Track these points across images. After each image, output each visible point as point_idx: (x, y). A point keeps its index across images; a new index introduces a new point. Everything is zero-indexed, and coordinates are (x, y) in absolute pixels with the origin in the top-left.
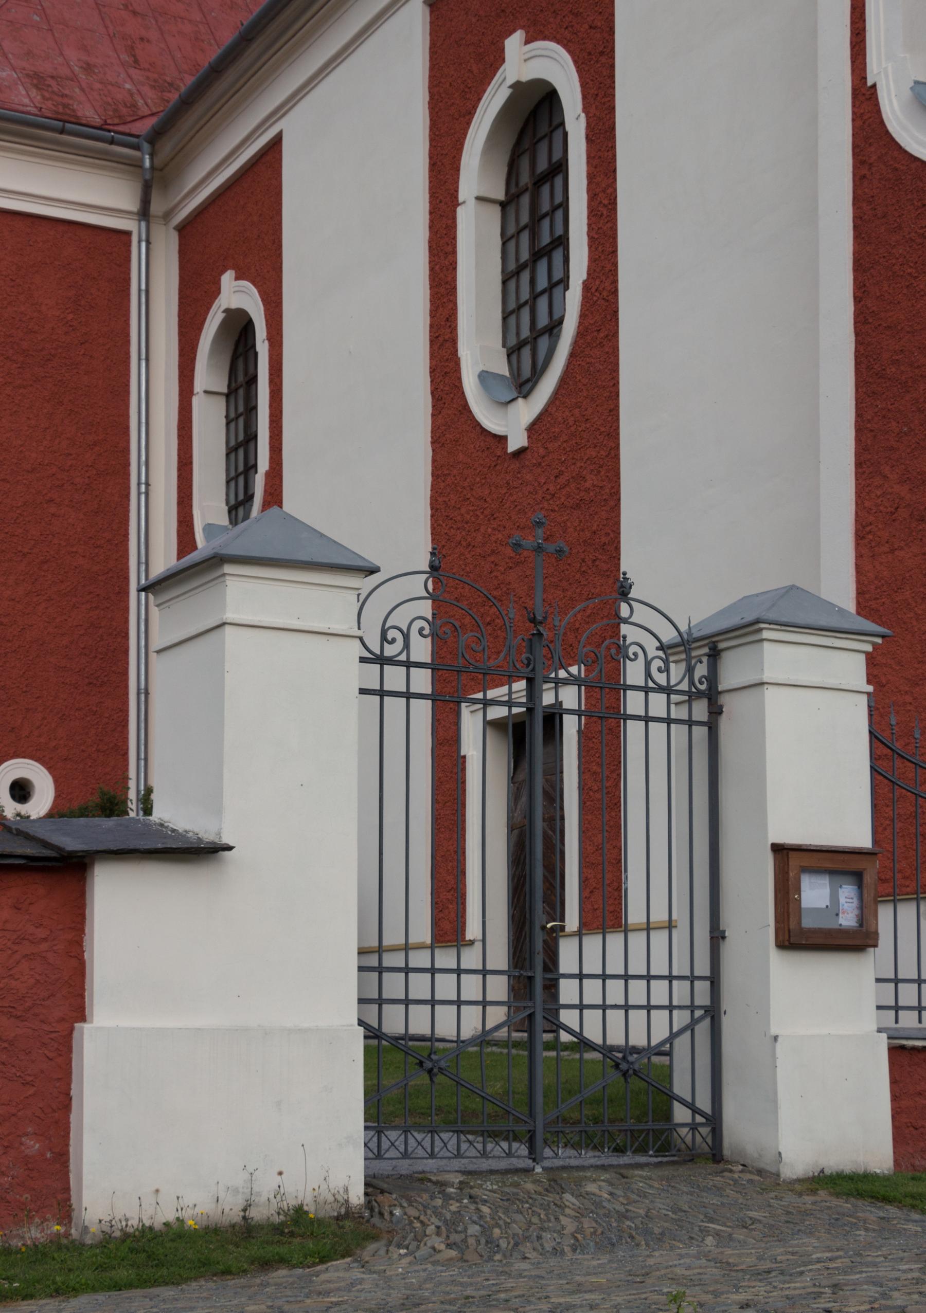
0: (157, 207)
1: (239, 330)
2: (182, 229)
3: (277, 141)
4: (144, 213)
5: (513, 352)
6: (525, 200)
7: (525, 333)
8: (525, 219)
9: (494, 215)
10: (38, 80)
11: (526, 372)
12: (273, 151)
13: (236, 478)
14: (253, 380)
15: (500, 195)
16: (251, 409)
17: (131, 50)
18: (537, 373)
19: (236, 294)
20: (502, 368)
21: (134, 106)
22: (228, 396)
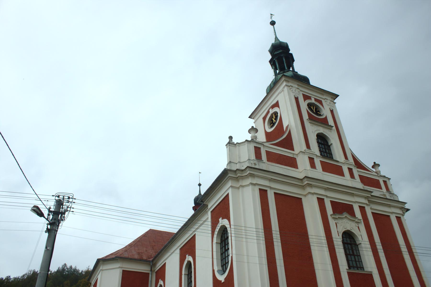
0: (153, 269)
1: (189, 263)
2: (156, 272)
3: (165, 263)
4: (151, 270)
5: (222, 266)
6: (223, 242)
7: (224, 263)
8: (224, 245)
9: (187, 276)
10: (139, 253)
11: (225, 270)
12: (194, 237)
13: (223, 260)
14: (191, 272)
15: (220, 242)
16: (191, 277)
17: (153, 248)
18: (226, 269)
19: (189, 258)
20: (221, 269)
21: (151, 256)
22: (220, 244)
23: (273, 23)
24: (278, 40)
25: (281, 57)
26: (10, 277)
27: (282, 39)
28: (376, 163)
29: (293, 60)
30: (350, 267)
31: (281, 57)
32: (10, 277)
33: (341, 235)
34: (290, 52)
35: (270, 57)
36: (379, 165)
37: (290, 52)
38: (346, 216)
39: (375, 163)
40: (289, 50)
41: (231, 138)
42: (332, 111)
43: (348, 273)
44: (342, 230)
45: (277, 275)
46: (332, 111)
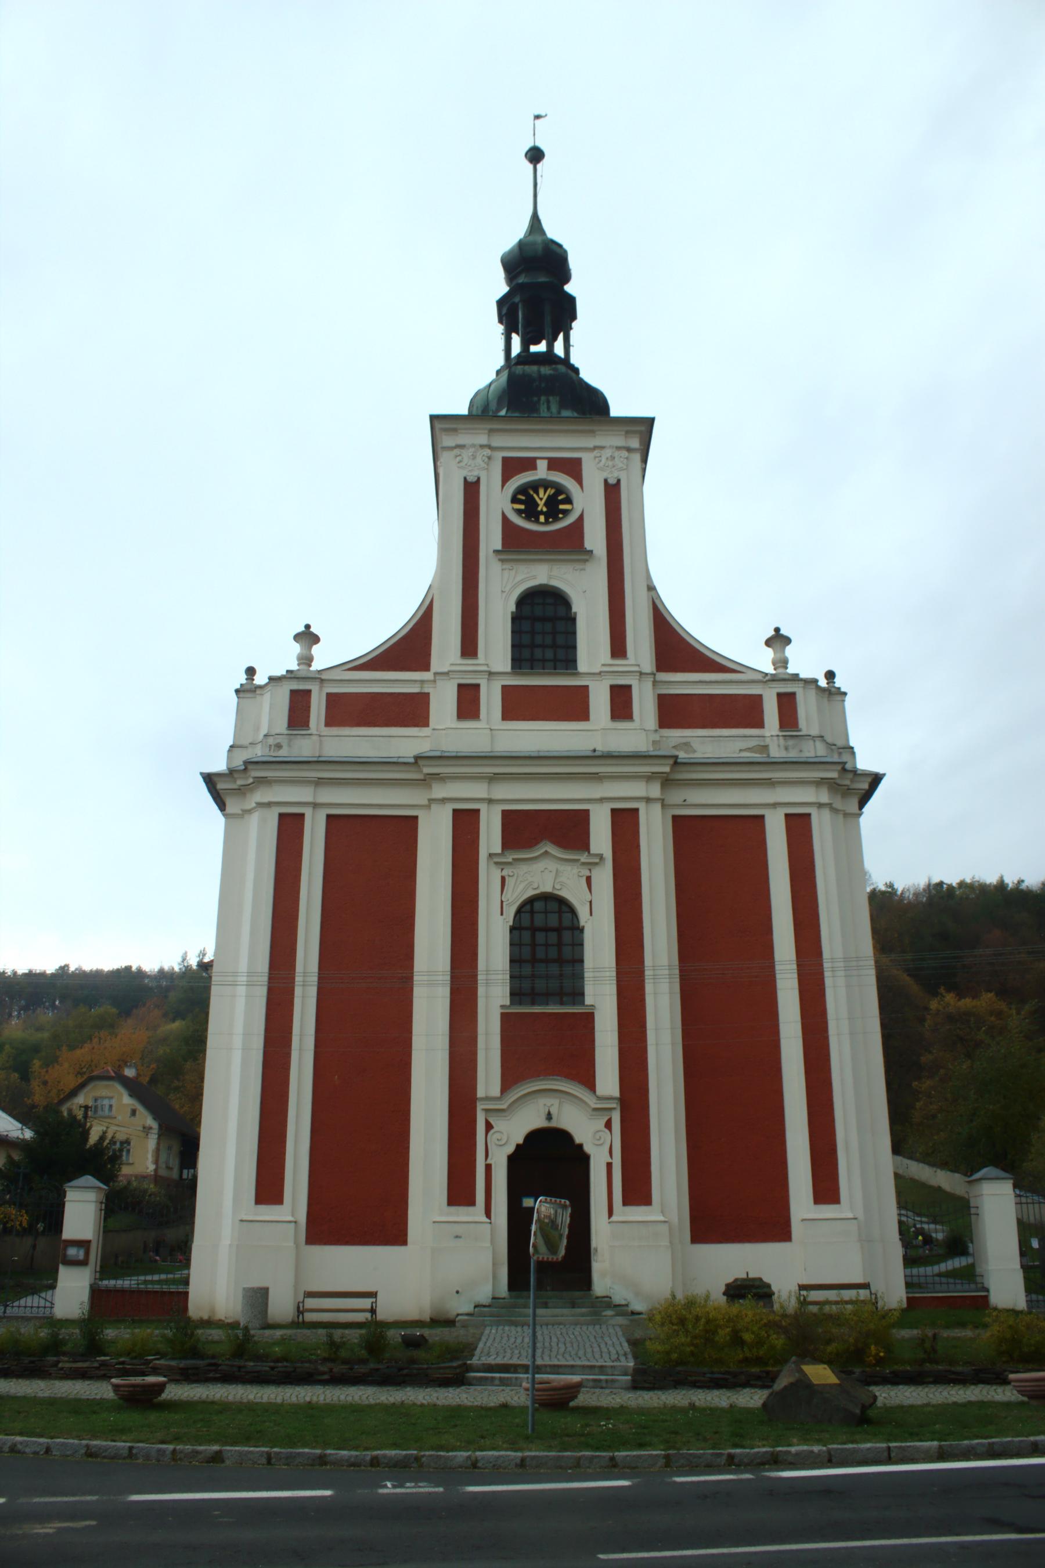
23: (535, 155)
24: (542, 232)
25: (537, 288)
26: (67, 966)
27: (539, 144)
28: (782, 632)
29: (574, 317)
30: (516, 995)
31: (537, 288)
32: (67, 966)
33: (511, 912)
34: (568, 288)
35: (502, 288)
36: (787, 641)
37: (568, 288)
38: (546, 852)
39: (777, 630)
40: (565, 275)
41: (251, 672)
42: (612, 492)
43: (505, 1018)
44: (519, 892)
45: (285, 1136)
46: (612, 492)
